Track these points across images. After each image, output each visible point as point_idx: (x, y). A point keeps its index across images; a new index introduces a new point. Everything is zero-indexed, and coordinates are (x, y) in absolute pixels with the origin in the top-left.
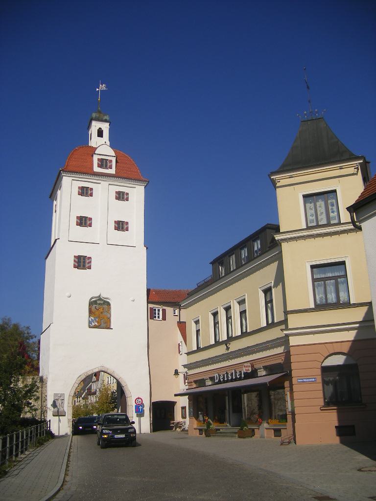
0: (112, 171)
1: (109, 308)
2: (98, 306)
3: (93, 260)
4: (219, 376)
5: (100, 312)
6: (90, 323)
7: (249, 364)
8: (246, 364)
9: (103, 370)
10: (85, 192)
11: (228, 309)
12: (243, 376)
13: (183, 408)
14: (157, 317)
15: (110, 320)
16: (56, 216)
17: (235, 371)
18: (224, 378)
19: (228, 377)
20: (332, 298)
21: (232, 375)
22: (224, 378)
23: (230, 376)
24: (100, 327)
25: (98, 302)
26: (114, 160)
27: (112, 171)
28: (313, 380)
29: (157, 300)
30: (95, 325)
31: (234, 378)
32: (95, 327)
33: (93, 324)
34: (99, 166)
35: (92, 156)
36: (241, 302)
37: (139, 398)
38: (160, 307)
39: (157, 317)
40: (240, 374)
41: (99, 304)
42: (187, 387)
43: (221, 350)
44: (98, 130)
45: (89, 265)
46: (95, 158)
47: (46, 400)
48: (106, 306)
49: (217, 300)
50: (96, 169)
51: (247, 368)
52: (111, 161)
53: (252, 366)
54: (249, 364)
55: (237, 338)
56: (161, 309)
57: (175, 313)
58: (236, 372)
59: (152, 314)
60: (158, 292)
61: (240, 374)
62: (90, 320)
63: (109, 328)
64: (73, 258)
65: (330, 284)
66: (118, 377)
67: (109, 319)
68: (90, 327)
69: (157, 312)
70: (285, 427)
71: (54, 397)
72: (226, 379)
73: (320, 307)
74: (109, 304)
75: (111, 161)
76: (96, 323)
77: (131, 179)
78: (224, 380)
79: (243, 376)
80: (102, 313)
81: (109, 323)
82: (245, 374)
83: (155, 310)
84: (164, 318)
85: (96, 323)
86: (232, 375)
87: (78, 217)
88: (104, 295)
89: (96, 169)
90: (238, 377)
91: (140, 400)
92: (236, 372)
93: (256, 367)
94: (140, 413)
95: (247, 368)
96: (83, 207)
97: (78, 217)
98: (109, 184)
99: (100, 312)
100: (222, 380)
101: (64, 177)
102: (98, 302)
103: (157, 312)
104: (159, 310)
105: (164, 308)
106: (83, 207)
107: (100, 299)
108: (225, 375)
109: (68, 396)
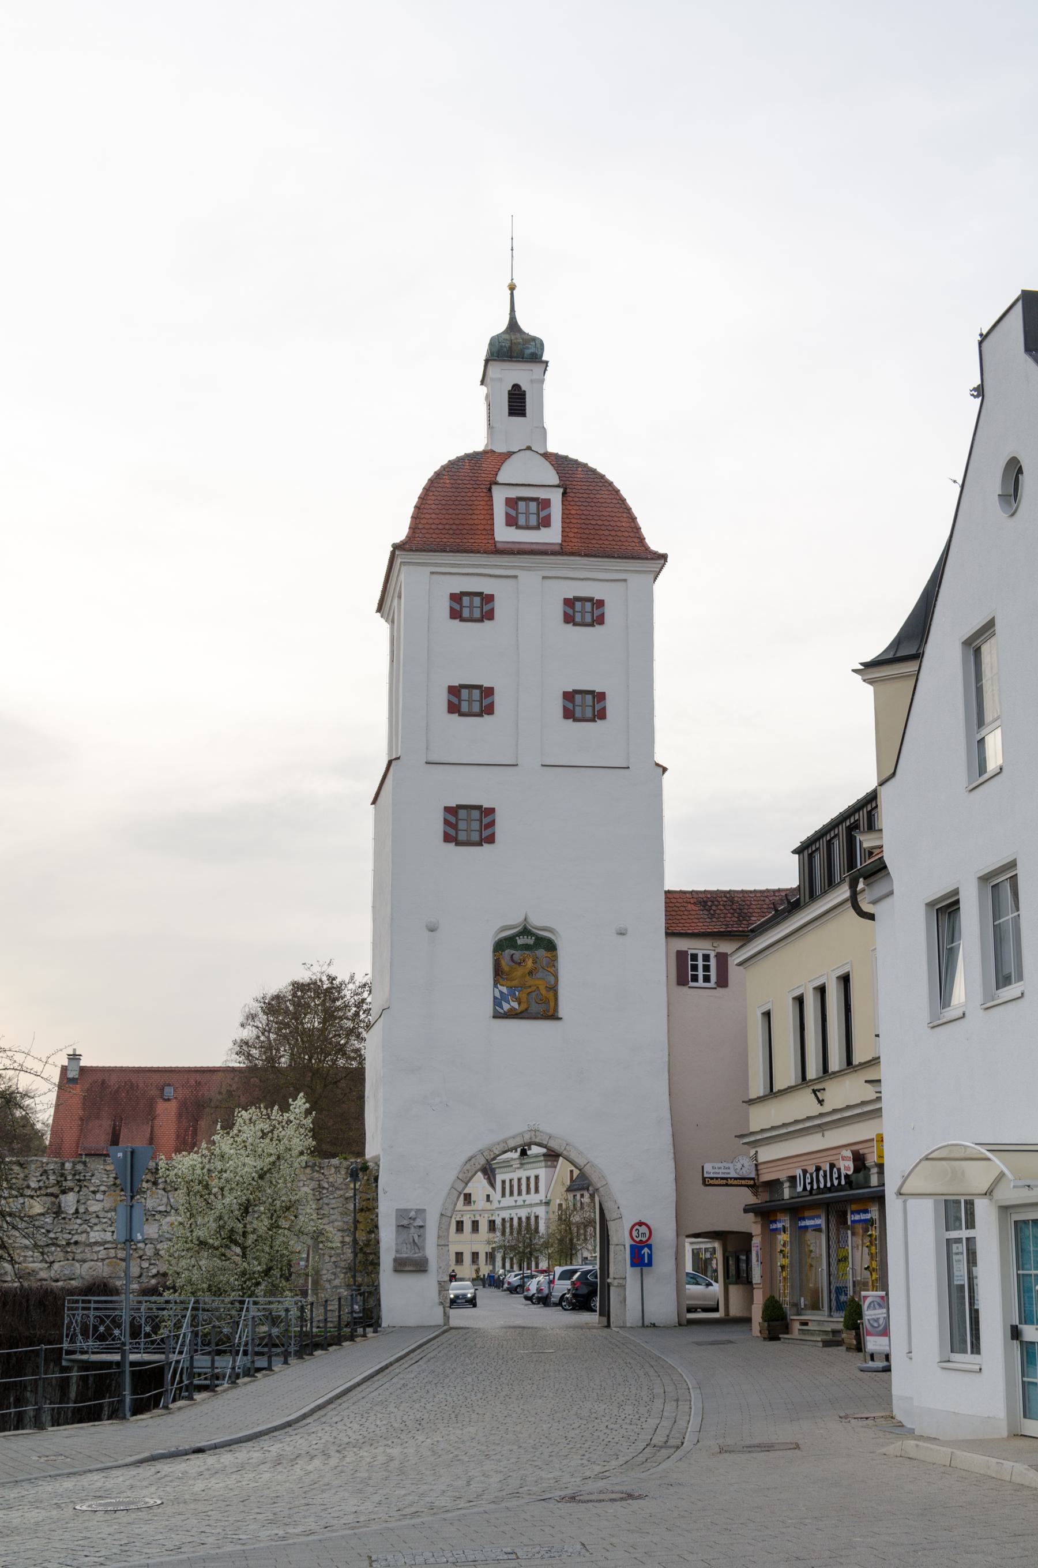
0: (552, 535)
1: (554, 960)
2: (518, 955)
6: (497, 1003)
7: (849, 1154)
9: (537, 1140)
11: (822, 990)
12: (843, 1182)
14: (701, 978)
16: (399, 605)
25: (520, 941)
26: (556, 497)
27: (552, 535)
29: (700, 928)
30: (512, 1009)
31: (829, 1185)
32: (512, 1015)
33: (506, 1007)
34: (511, 521)
35: (490, 490)
37: (641, 1224)
39: (701, 978)
41: (526, 947)
42: (843, 1172)
44: (510, 393)
46: (499, 497)
47: (377, 1227)
48: (541, 953)
50: (504, 534)
52: (545, 504)
56: (712, 954)
59: (685, 972)
62: (498, 995)
63: (552, 1015)
64: (439, 816)
66: (581, 1162)
67: (554, 989)
68: (497, 1016)
69: (700, 963)
70: (834, 1308)
71: (397, 1219)
74: (550, 946)
75: (545, 504)
76: (515, 1005)
79: (843, 1182)
80: (531, 973)
81: (552, 1004)
83: (694, 957)
85: (515, 1005)
88: (537, 921)
89: (504, 534)
91: (643, 1229)
98: (544, 578)
103: (700, 963)
104: (706, 958)
107: (526, 931)
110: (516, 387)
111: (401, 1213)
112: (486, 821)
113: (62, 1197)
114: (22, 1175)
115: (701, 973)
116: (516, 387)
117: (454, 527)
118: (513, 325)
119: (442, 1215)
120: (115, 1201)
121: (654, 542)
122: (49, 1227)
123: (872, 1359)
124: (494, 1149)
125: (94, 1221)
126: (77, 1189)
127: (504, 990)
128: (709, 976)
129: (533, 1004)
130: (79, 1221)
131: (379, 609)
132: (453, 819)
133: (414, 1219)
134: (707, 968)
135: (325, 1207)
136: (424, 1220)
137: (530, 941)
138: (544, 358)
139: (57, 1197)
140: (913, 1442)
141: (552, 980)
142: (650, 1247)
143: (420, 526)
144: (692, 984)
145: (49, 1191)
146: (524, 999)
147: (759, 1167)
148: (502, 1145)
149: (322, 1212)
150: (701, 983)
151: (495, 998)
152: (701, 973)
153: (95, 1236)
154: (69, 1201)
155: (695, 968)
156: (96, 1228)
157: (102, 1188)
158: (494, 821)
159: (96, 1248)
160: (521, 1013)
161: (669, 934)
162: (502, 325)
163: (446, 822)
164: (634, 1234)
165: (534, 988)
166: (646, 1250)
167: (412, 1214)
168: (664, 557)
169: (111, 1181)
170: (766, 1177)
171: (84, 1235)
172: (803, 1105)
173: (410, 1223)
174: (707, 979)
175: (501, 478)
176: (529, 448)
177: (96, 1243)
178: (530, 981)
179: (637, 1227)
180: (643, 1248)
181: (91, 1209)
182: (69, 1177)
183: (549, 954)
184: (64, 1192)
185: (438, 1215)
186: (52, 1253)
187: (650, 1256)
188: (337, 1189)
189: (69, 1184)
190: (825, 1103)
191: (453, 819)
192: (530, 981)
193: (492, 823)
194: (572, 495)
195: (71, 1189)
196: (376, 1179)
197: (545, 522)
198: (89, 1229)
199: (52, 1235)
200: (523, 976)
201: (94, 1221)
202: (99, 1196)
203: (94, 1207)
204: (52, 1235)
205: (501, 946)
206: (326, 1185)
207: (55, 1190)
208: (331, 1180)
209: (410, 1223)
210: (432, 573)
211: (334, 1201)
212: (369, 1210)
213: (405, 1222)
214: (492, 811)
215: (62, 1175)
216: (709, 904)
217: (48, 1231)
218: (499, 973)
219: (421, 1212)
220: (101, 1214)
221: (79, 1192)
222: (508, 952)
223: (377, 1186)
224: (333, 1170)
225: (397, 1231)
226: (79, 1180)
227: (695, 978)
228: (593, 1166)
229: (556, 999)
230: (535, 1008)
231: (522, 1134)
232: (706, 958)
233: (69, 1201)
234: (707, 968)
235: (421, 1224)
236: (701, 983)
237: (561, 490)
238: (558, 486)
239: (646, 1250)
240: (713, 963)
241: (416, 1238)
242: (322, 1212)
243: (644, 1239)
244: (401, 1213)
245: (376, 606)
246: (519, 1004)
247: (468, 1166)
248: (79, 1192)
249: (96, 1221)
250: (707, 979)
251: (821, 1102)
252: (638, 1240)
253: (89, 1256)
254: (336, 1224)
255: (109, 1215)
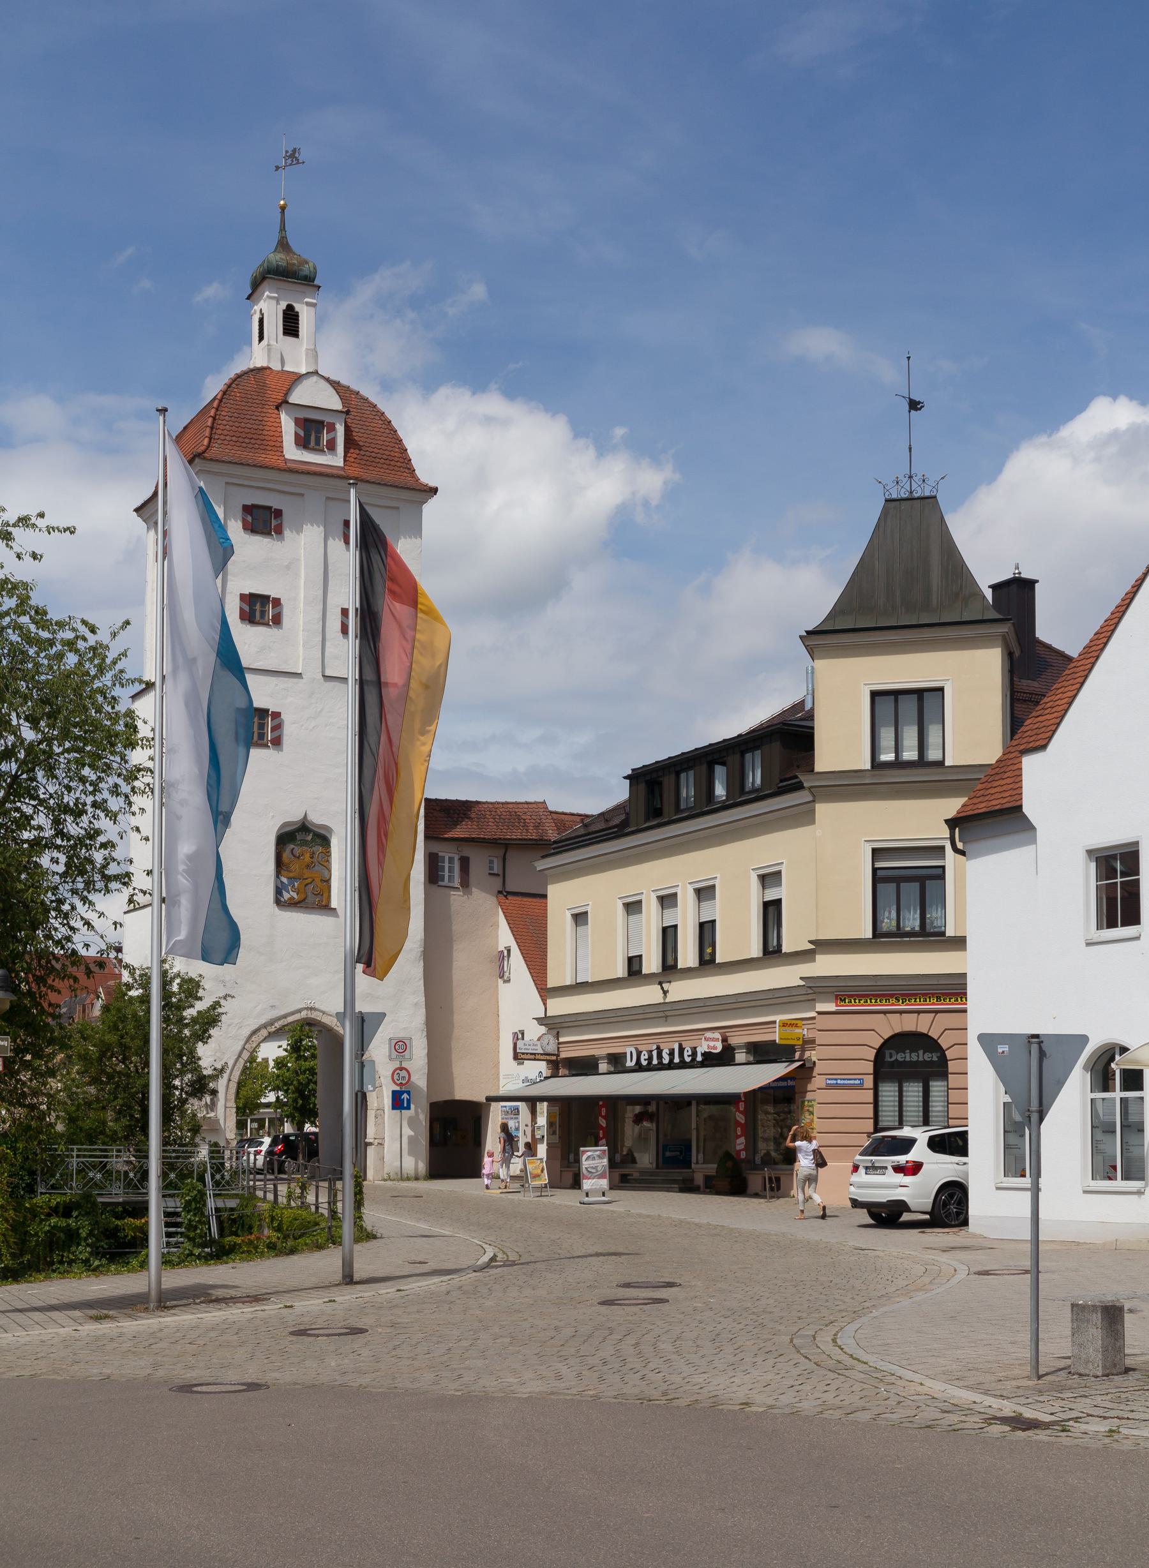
4: (639, 1054)
6: (278, 892)
8: (709, 1035)
12: (699, 1058)
13: (400, 1047)
15: (329, 887)
17: (680, 1045)
18: (650, 1059)
19: (660, 1056)
20: (912, 921)
21: (671, 1054)
22: (650, 1059)
27: (336, 460)
28: (857, 1082)
30: (292, 898)
32: (293, 905)
33: (286, 896)
34: (303, 442)
36: (705, 893)
40: (694, 1054)
43: (668, 1013)
45: (276, 734)
49: (646, 878)
51: (712, 1044)
53: (725, 1040)
54: (717, 1035)
55: (688, 972)
56: (456, 858)
57: (491, 868)
58: (681, 1050)
61: (694, 1054)
65: (911, 891)
72: (655, 1062)
73: (882, 938)
75: (332, 428)
76: (295, 895)
79: (699, 1058)
80: (308, 866)
82: (704, 1054)
85: (295, 895)
86: (671, 1054)
87: (243, 597)
88: (316, 818)
90: (688, 1059)
91: (403, 1073)
92: (681, 1050)
93: (734, 1041)
95: (712, 1044)
97: (243, 597)
98: (328, 498)
100: (644, 1063)
104: (451, 860)
108: (655, 1053)
121: (425, 476)
123: (587, 1195)
127: (285, 880)
140: (505, 937)
160: (300, 902)
164: (396, 1077)
165: (309, 880)
166: (405, 1096)
168: (434, 491)
176: (316, 373)
178: (307, 873)
187: (409, 1101)
192: (307, 873)
194: (221, 427)
245: (139, 504)
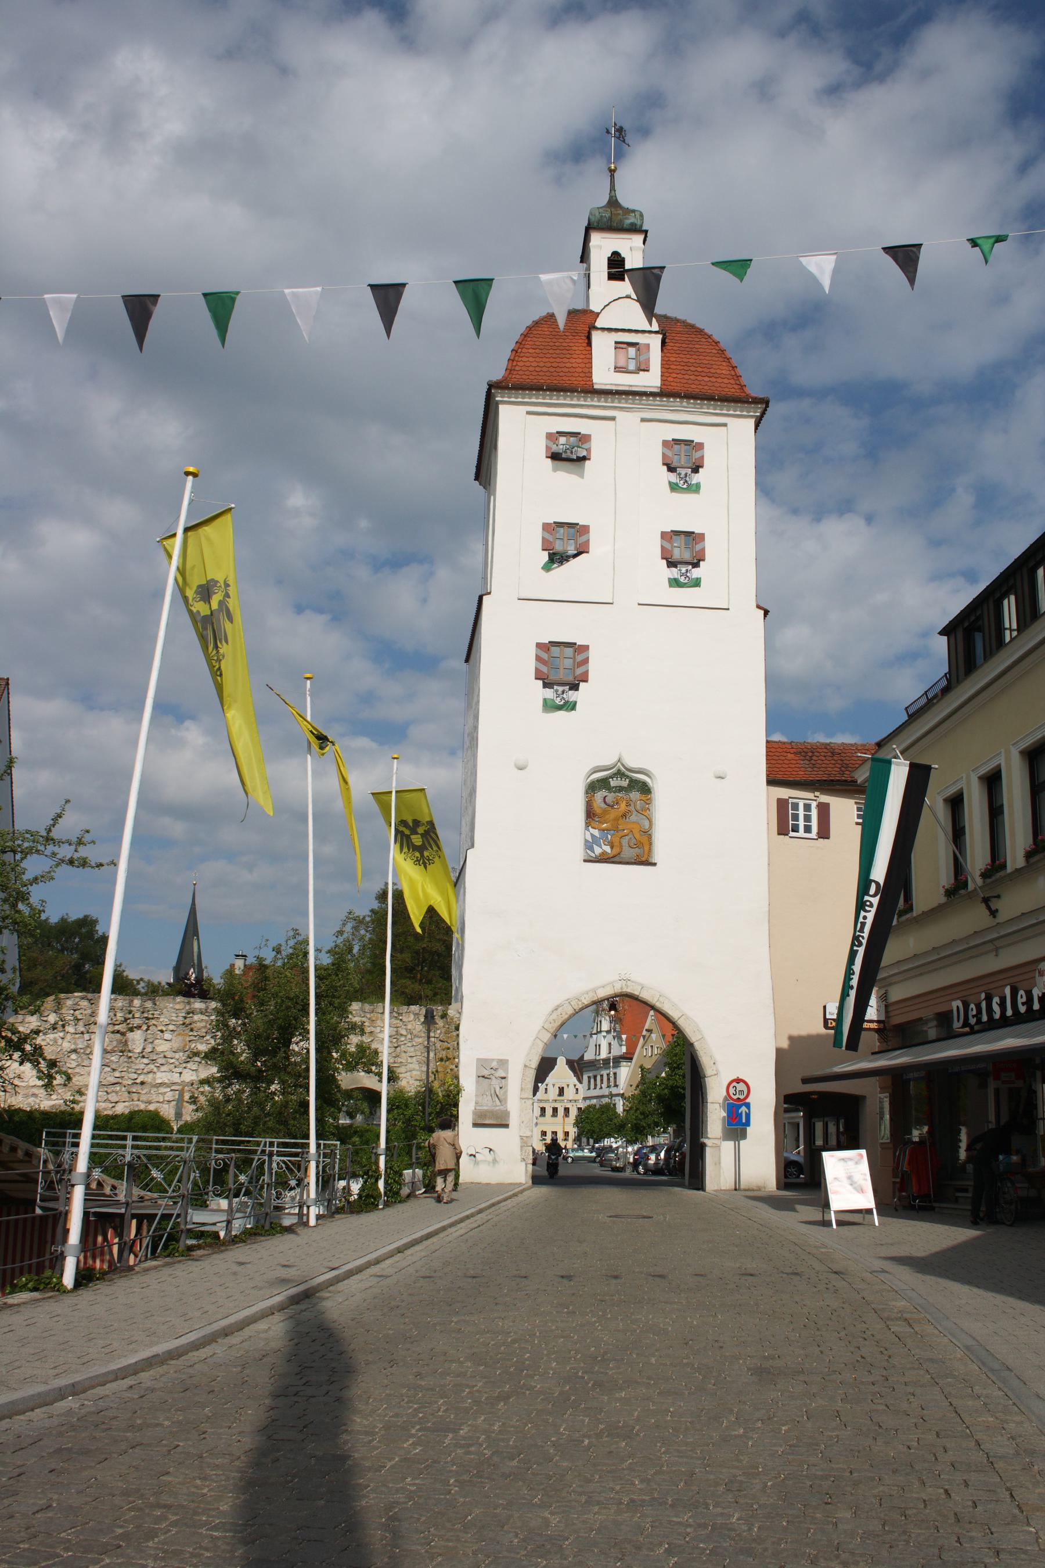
0: (652, 380)
1: (648, 802)
2: (611, 797)
3: (592, 654)
5: (619, 813)
6: (589, 846)
10: (569, 454)
11: (993, 781)
12: (1036, 1006)
14: (801, 828)
15: (650, 837)
23: (996, 1008)
24: (617, 859)
25: (613, 783)
26: (655, 342)
29: (800, 776)
30: (604, 853)
31: (1009, 1012)
33: (598, 851)
37: (738, 1081)
38: (810, 795)
39: (801, 828)
41: (620, 789)
44: (609, 259)
48: (635, 795)
50: (603, 375)
56: (814, 804)
59: (785, 822)
60: (808, 753)
64: (532, 651)
67: (648, 834)
69: (801, 812)
71: (477, 1069)
74: (645, 789)
76: (608, 849)
77: (710, 398)
78: (979, 1021)
79: (1036, 1006)
80: (624, 816)
81: (646, 849)
83: (795, 807)
84: (824, 833)
85: (608, 849)
88: (632, 762)
91: (741, 1086)
94: (737, 1124)
96: (565, 496)
99: (619, 813)
101: (501, 407)
102: (613, 783)
103: (801, 812)
104: (807, 808)
105: (824, 798)
106: (565, 496)
108: (984, 1005)
109: (521, 1067)
110: (616, 254)
111: (482, 1063)
112: (580, 658)
113: (130, 1035)
114: (89, 1011)
115: (801, 823)
116: (616, 254)
117: (552, 370)
118: (613, 203)
119: (526, 1066)
120: (184, 1040)
122: (114, 1066)
124: (582, 998)
125: (161, 1061)
126: (145, 1027)
128: (810, 826)
129: (626, 848)
130: (146, 1061)
131: (477, 478)
132: (545, 656)
133: (496, 1070)
134: (808, 818)
135: (403, 1054)
136: (506, 1071)
137: (625, 783)
138: (644, 228)
139: (123, 1034)
141: (647, 824)
142: (748, 1106)
143: (517, 368)
144: (792, 834)
145: (117, 1028)
146: (616, 844)
147: (890, 1009)
148: (591, 994)
149: (400, 1060)
150: (801, 833)
151: (586, 841)
152: (801, 823)
153: (161, 1077)
154: (136, 1040)
155: (796, 817)
156: (163, 1068)
157: (171, 1027)
158: (588, 658)
159: (162, 1090)
161: (771, 782)
162: (604, 200)
163: (538, 658)
164: (732, 1091)
166: (743, 1109)
167: (494, 1064)
169: (181, 1020)
170: (897, 1020)
171: (151, 1075)
172: (970, 919)
173: (491, 1073)
174: (808, 829)
175: (598, 324)
177: (161, 1084)
179: (734, 1084)
180: (741, 1106)
181: (159, 1049)
182: (137, 1015)
183: (643, 797)
184: (131, 1030)
185: (521, 1066)
186: (117, 1093)
187: (748, 1116)
188: (416, 1036)
189: (136, 1022)
190: (999, 915)
191: (545, 656)
193: (586, 661)
195: (139, 1027)
196: (457, 1028)
197: (643, 368)
198: (155, 1069)
199: (117, 1074)
200: (616, 819)
201: (161, 1061)
202: (167, 1036)
203: (162, 1047)
204: (117, 1074)
205: (592, 788)
206: (404, 1032)
207: (121, 1028)
208: (409, 1027)
209: (491, 1073)
210: (528, 413)
211: (412, 1049)
212: (448, 1059)
213: (486, 1073)
214: (585, 648)
215: (130, 1012)
216: (810, 754)
217: (114, 1070)
218: (590, 815)
219: (503, 1063)
220: (169, 1054)
221: (147, 1030)
222: (599, 795)
223: (458, 1035)
224: (412, 1017)
225: (477, 1082)
226: (147, 1019)
227: (795, 829)
228: (688, 1018)
229: (651, 844)
230: (628, 853)
231: (612, 983)
232: (807, 808)
233: (136, 1040)
234: (808, 818)
235: (503, 1075)
236: (801, 833)
237: (660, 336)
238: (656, 332)
239: (743, 1109)
240: (814, 814)
241: (498, 1089)
242: (400, 1060)
243: (742, 1097)
244: (482, 1063)
245: (473, 470)
246: (612, 848)
247: (554, 1016)
248: (147, 1030)
249: (163, 1061)
250: (808, 829)
251: (994, 913)
252: (735, 1097)
253: (155, 1098)
254: (414, 1073)
255: (177, 1056)
